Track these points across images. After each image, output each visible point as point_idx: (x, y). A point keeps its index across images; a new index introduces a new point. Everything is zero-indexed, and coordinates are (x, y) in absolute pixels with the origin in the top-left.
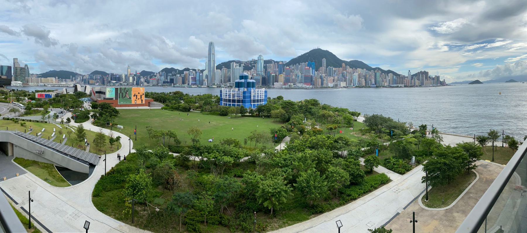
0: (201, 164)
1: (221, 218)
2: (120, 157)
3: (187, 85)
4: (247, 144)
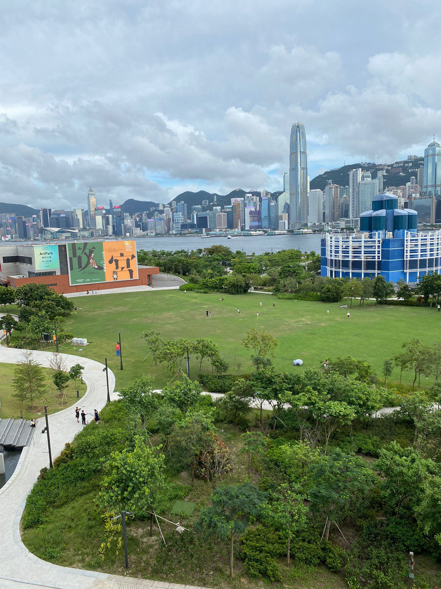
0: (276, 419)
1: (323, 549)
2: (83, 415)
3: (240, 229)
4: (392, 374)
